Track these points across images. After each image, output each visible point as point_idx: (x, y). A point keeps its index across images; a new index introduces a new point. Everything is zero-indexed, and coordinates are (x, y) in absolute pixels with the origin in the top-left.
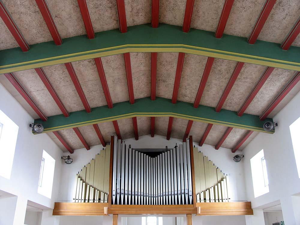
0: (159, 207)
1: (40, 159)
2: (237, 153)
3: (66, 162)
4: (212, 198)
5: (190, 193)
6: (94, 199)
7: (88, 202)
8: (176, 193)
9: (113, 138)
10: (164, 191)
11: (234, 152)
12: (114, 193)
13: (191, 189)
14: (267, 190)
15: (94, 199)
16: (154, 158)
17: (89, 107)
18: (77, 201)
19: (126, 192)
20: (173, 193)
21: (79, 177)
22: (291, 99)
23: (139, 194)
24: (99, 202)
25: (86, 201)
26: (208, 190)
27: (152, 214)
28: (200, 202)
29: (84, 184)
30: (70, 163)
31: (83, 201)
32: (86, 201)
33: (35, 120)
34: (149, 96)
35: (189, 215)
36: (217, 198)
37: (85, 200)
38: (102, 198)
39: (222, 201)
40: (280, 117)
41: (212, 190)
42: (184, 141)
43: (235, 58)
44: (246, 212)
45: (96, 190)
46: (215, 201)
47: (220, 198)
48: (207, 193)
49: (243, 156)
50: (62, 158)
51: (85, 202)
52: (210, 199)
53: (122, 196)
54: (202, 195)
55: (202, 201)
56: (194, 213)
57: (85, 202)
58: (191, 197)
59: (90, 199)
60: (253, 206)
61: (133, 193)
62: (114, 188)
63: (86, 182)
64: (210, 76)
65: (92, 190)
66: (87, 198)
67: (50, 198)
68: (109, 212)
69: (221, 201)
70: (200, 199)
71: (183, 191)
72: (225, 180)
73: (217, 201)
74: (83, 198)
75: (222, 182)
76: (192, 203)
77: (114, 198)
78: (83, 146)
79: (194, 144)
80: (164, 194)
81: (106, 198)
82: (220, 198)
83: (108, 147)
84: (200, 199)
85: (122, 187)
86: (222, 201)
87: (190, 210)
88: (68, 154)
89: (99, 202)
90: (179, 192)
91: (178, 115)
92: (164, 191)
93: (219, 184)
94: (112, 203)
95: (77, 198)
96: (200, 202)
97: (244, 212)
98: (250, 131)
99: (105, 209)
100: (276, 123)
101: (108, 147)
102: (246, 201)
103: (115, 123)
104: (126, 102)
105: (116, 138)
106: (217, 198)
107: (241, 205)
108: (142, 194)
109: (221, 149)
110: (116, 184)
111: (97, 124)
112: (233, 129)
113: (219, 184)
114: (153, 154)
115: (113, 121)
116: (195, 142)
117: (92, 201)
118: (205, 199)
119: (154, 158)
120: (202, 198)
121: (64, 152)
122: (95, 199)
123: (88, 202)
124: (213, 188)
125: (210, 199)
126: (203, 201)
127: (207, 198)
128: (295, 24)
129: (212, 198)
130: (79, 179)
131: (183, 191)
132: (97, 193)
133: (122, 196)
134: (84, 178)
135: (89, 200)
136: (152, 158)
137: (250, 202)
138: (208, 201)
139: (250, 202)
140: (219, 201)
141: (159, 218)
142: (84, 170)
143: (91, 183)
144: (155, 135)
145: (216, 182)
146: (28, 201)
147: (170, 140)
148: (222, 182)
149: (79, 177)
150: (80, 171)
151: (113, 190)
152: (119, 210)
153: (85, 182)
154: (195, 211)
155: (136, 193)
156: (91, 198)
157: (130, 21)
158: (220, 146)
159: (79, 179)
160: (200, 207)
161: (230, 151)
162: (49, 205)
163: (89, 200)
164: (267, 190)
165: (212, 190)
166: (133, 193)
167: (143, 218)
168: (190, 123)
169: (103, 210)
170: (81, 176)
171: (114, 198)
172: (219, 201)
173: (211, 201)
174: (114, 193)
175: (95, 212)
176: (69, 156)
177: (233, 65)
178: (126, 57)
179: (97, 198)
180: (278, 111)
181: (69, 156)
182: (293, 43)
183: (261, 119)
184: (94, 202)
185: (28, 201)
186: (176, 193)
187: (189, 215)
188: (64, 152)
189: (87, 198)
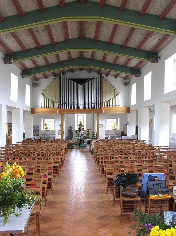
0: (85, 110)
1: (9, 78)
2: (126, 81)
3: (35, 86)
4: (111, 105)
5: (99, 103)
6: (51, 106)
7: (48, 107)
8: (92, 103)
9: (60, 74)
10: (86, 102)
11: (125, 80)
12: (61, 103)
13: (100, 101)
14: (135, 103)
15: (51, 106)
16: (82, 85)
17: (40, 45)
18: (42, 107)
19: (68, 103)
20: (91, 103)
21: (42, 94)
22: (167, 44)
23: (74, 103)
24: (54, 107)
25: (47, 107)
26: (109, 101)
27: (81, 113)
28: (105, 107)
29: (45, 98)
30: (37, 87)
31: (45, 107)
32: (47, 107)
33: (22, 71)
34: (79, 57)
35: (98, 114)
36: (113, 105)
37: (46, 106)
38: (55, 105)
39: (116, 107)
40: (162, 54)
41: (111, 101)
42: (98, 74)
43: (131, 25)
44: (127, 112)
45: (52, 101)
46: (112, 107)
47: (115, 105)
48: (109, 102)
49: (129, 83)
50: (32, 84)
51: (46, 107)
52: (110, 105)
53: (66, 105)
54: (106, 103)
55: (105, 107)
56: (101, 113)
57: (46, 107)
58: (100, 105)
59: (49, 106)
60: (131, 109)
61: (71, 103)
62: (61, 101)
63: (46, 97)
64: (107, 57)
65: (50, 101)
66: (47, 105)
67: (30, 106)
68: (59, 112)
69: (115, 106)
70: (105, 105)
71: (96, 102)
72: (118, 95)
73: (113, 106)
74: (45, 105)
75: (117, 96)
76: (100, 108)
77: (61, 105)
78: (43, 77)
79: (103, 75)
80: (86, 103)
81: (57, 105)
82: (115, 105)
83: (57, 78)
84: (105, 105)
85: (66, 100)
86: (116, 107)
87: (99, 111)
88: (35, 82)
89: (54, 107)
90: (94, 103)
91: (103, 19)
92: (86, 102)
93: (115, 98)
94: (61, 108)
95: (42, 105)
96: (105, 107)
97: (126, 112)
98: (128, 75)
99: (57, 111)
100: (159, 57)
101: (57, 78)
102: (128, 107)
103: (57, 56)
104: (68, 60)
105: (62, 74)
106: (113, 105)
107: (125, 108)
108: (75, 103)
109: (118, 78)
110: (63, 98)
111: (46, 56)
112: (11, 233)
113: (115, 98)
114: (81, 81)
115: (56, 54)
116: (104, 74)
117: (50, 107)
118: (107, 105)
119: (82, 85)
120: (106, 105)
121: (33, 80)
122: (52, 106)
123: (48, 107)
124: (111, 100)
125: (110, 105)
126: (106, 107)
127: (108, 105)
128: (166, 7)
129: (111, 105)
130: (43, 95)
131: (96, 102)
132: (52, 103)
133: (66, 105)
134: (45, 95)
135: (48, 106)
136: (81, 85)
137: (130, 107)
138: (108, 106)
139: (130, 107)
140: (114, 107)
141: (84, 114)
142: (45, 91)
143: (49, 97)
144: (82, 70)
145: (114, 96)
146: (23, 110)
147: (91, 73)
148: (117, 96)
149: (42, 94)
150: (42, 91)
151: (61, 102)
152: (64, 112)
153: (46, 97)
154: (101, 112)
155: (73, 103)
156: (50, 105)
157: (71, 37)
158: (118, 77)
159: (43, 95)
160: (103, 110)
161: (123, 79)
162: (29, 110)
163: (48, 106)
164: (135, 103)
165: (111, 101)
166: (71, 103)
167: (76, 115)
168: (105, 55)
169: (57, 111)
170: (43, 94)
171: (61, 105)
172: (114, 107)
173: (110, 106)
174: (61, 103)
175: (52, 112)
176: (36, 83)
177: (129, 30)
178: (65, 24)
179: (52, 105)
180: (161, 50)
181: (36, 83)
182: (166, 16)
183: (150, 53)
184: (51, 107)
185: (23, 110)
186: (92, 103)
187: (98, 114)
188: (33, 80)
189: (47, 105)
